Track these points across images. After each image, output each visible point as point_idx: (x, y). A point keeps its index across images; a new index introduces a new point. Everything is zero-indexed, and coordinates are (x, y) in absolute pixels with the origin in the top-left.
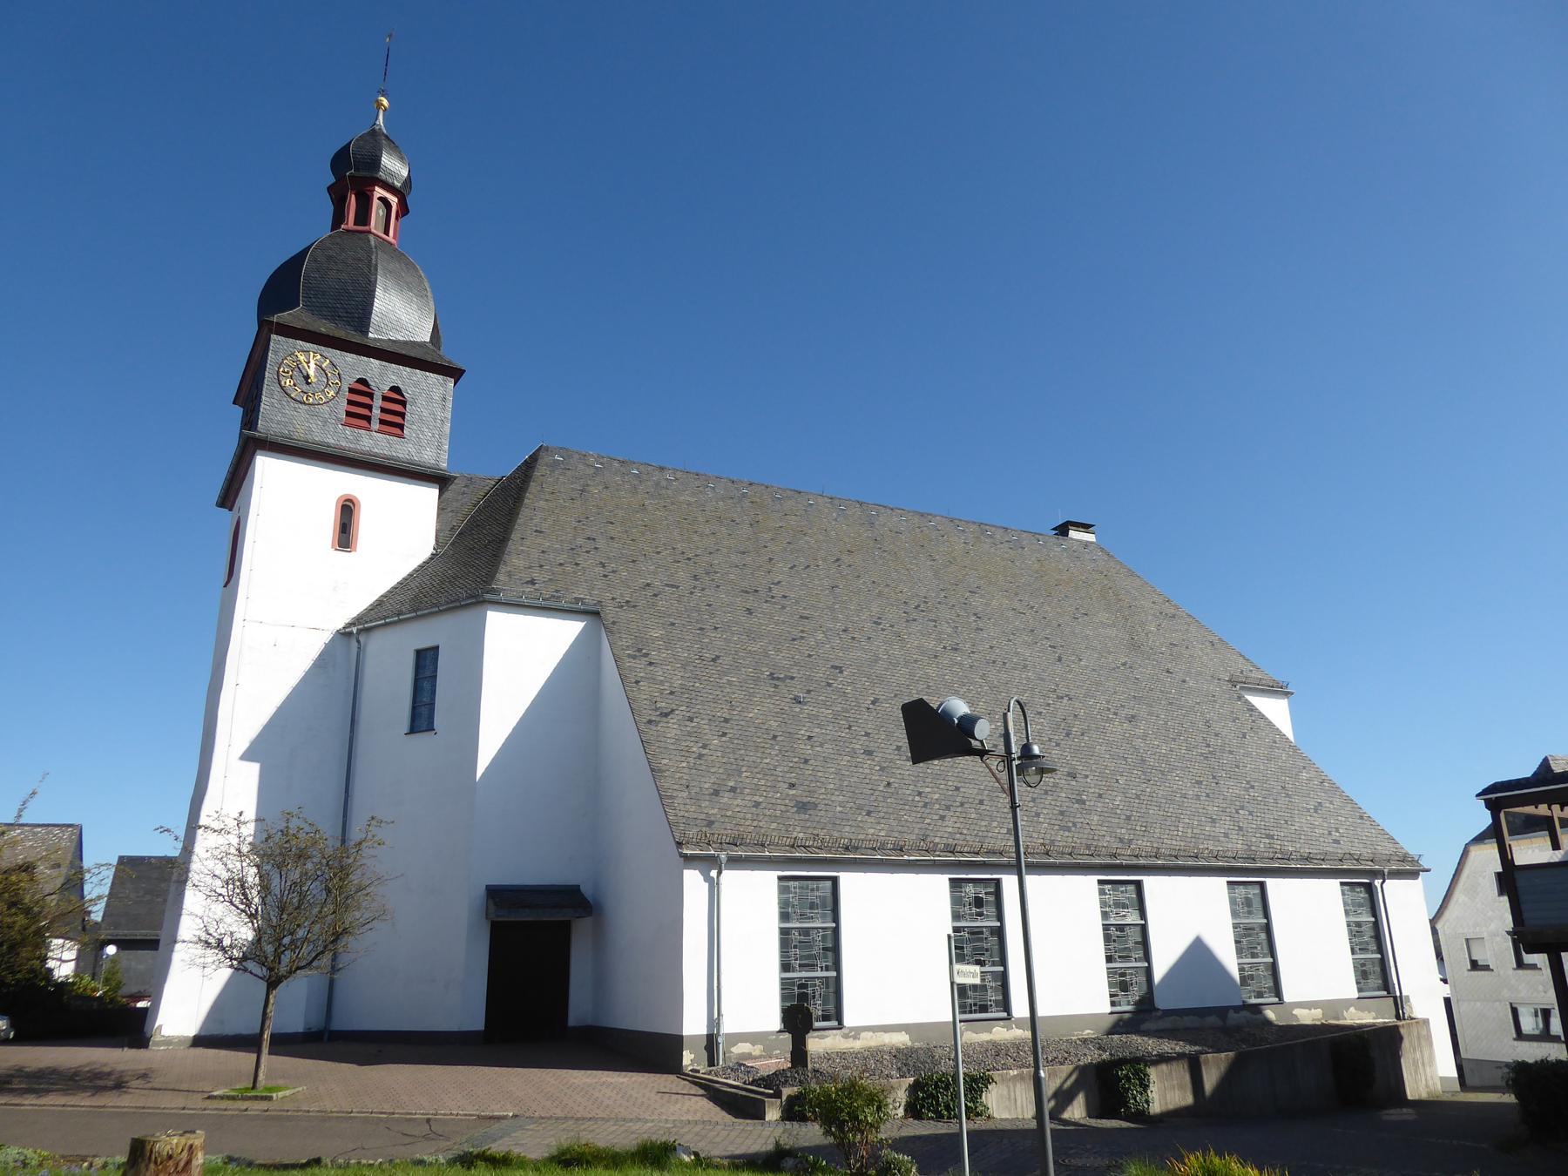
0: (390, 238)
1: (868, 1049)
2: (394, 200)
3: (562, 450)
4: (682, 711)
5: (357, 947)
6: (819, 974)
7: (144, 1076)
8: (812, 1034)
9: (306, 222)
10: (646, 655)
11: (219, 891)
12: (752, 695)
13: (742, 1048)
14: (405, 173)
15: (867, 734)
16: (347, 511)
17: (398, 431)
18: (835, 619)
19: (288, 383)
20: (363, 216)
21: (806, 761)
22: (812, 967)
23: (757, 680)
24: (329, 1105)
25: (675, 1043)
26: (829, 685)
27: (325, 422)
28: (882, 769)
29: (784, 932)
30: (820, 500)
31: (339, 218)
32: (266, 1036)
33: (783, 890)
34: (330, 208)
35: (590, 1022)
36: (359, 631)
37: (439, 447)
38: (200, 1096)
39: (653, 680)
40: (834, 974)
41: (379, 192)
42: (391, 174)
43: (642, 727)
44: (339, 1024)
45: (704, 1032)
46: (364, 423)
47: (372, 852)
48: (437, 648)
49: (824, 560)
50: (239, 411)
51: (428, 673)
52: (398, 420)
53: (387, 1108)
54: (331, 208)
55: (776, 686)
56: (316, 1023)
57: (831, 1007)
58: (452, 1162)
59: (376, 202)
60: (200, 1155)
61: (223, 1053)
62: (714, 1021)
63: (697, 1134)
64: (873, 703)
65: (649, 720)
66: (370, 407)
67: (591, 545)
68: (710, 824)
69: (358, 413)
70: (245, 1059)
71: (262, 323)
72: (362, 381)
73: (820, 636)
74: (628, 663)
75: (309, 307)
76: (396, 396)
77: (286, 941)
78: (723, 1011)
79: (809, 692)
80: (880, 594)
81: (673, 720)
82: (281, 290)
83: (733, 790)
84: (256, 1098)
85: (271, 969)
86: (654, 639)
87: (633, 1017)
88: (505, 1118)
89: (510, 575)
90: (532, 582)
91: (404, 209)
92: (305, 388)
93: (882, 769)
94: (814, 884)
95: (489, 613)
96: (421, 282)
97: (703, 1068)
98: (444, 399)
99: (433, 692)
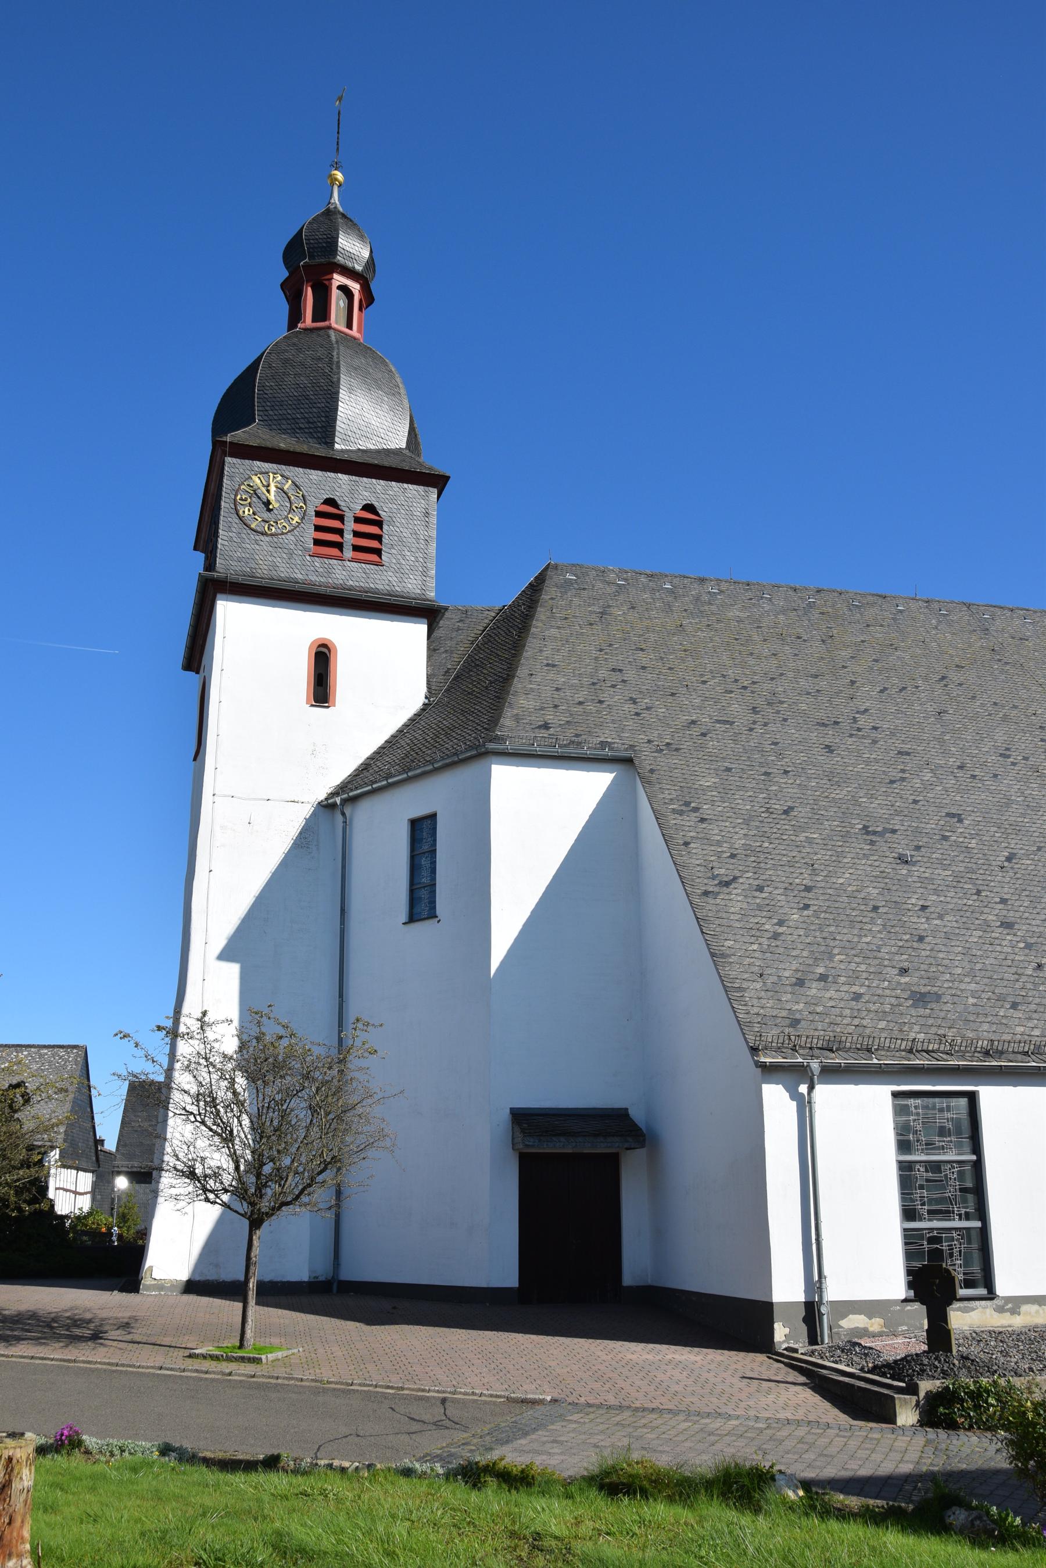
0: (354, 332)
1: (1034, 1328)
2: (355, 287)
3: (573, 567)
4: (747, 879)
5: (355, 1175)
6: (957, 1224)
7: (126, 1326)
8: (956, 1305)
9: (258, 324)
10: (696, 810)
11: (189, 1108)
12: (840, 855)
13: (855, 1321)
14: (366, 254)
15: (1003, 901)
16: (322, 659)
17: (374, 557)
18: (946, 753)
19: (247, 512)
20: (322, 311)
21: (921, 939)
22: (946, 1214)
23: (846, 836)
24: (326, 1374)
25: (762, 1313)
26: (945, 838)
27: (291, 554)
28: (1029, 946)
29: (905, 1169)
30: (913, 605)
31: (295, 316)
32: (252, 1284)
33: (900, 1111)
34: (284, 308)
35: (650, 1282)
36: (344, 801)
37: (425, 573)
38: (183, 1353)
39: (707, 840)
40: (978, 1224)
41: (338, 279)
42: (351, 257)
43: (696, 900)
44: (348, 1274)
45: (801, 1297)
46: (335, 551)
47: (362, 1063)
48: (433, 817)
49: (926, 679)
50: (201, 557)
51: (426, 847)
52: (374, 544)
53: (395, 1381)
54: (286, 307)
55: (872, 843)
56: (323, 1271)
57: (976, 1269)
58: (450, 1475)
59: (335, 293)
60: (25, 1472)
61: (217, 1302)
62: (814, 1283)
63: (801, 1441)
64: (1009, 859)
65: (704, 893)
66: (340, 532)
67: (617, 677)
68: (795, 1023)
69: (328, 542)
70: (229, 1309)
71: (216, 444)
72: (330, 502)
73: (928, 776)
74: (673, 820)
75: (269, 423)
76: (371, 516)
77: (267, 1169)
78: (826, 1271)
79: (918, 848)
80: (1005, 718)
81: (736, 890)
82: (236, 406)
83: (823, 978)
84: (242, 1359)
85: (252, 1204)
86: (705, 790)
87: (704, 1274)
88: (541, 1402)
89: (517, 718)
90: (546, 726)
91: (368, 298)
92: (266, 515)
93: (1029, 946)
94: (943, 1102)
95: (493, 766)
96: (392, 377)
97: (802, 1346)
98: (427, 514)
99: (433, 871)
